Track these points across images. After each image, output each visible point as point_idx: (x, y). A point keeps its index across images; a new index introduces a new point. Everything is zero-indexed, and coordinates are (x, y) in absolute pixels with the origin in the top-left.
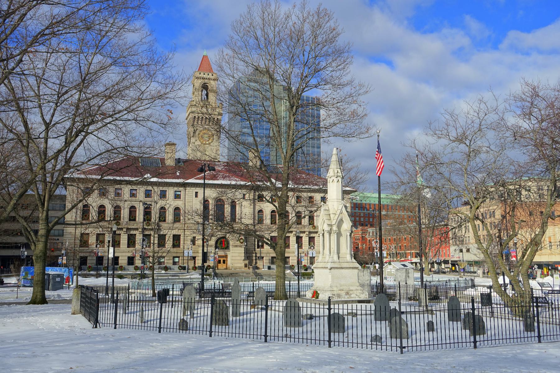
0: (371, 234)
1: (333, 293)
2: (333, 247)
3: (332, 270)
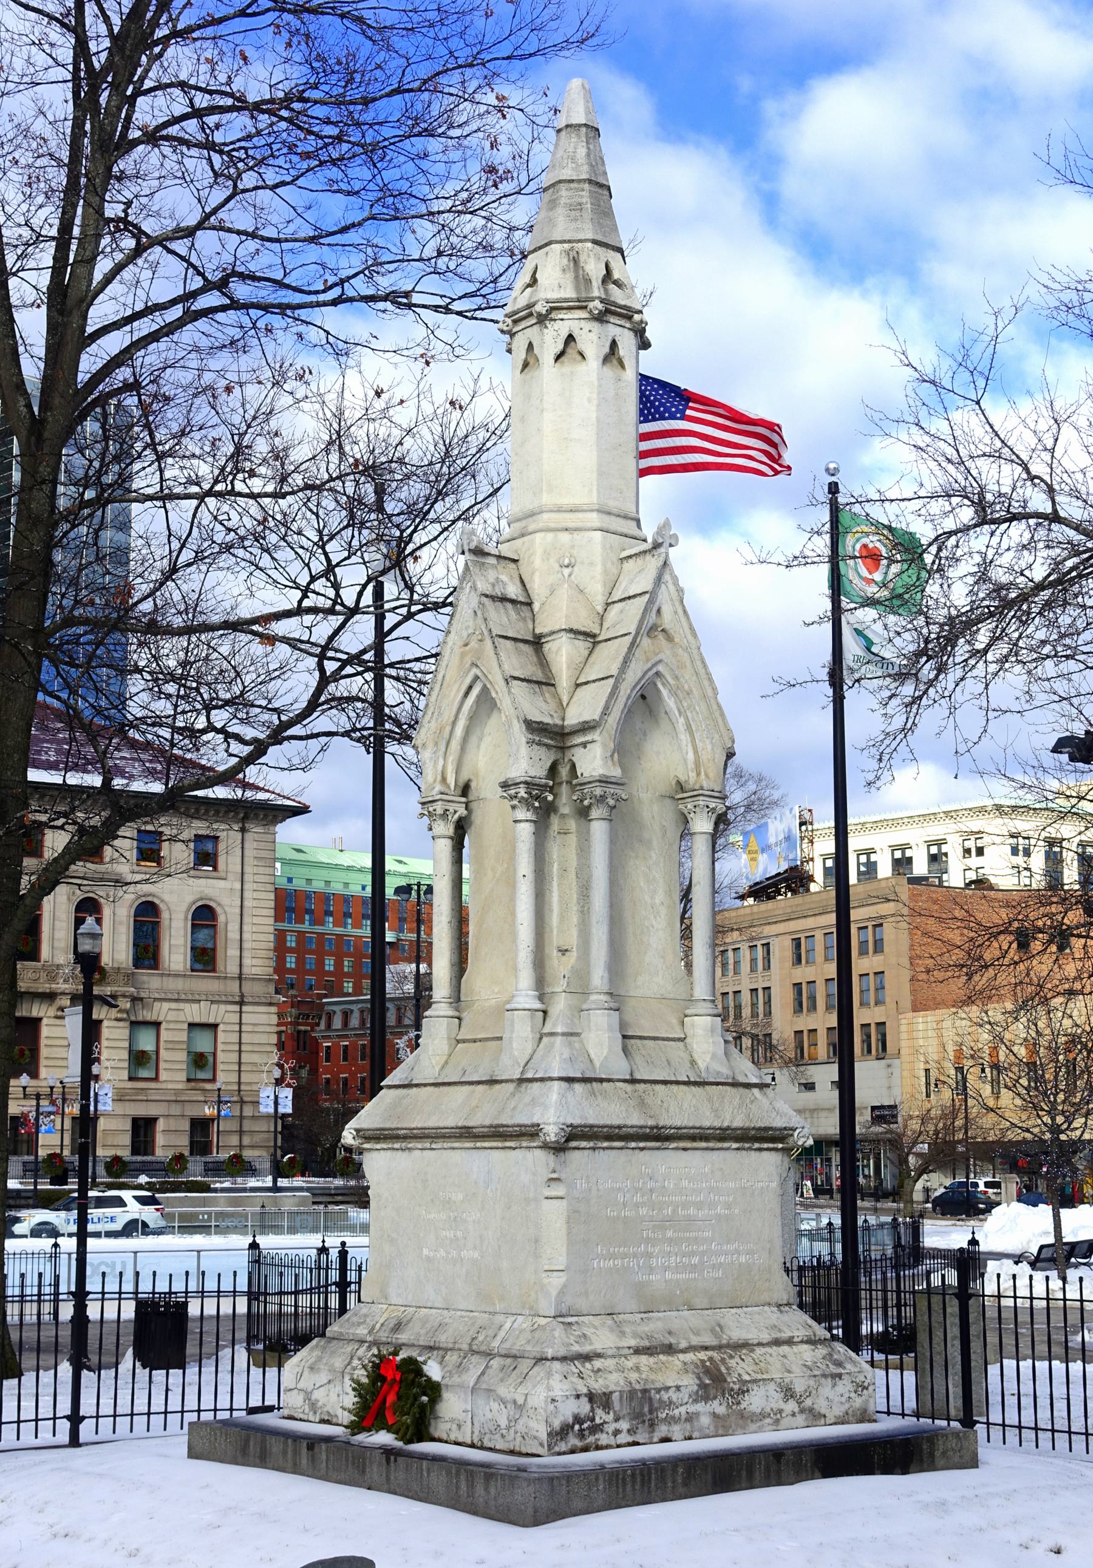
0: (337, 1023)
1: (598, 1385)
2: (572, 939)
3: (579, 1159)
